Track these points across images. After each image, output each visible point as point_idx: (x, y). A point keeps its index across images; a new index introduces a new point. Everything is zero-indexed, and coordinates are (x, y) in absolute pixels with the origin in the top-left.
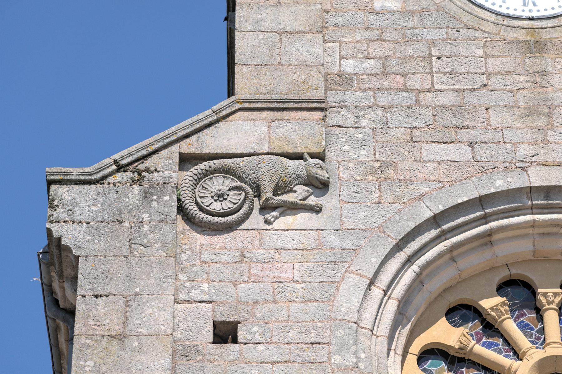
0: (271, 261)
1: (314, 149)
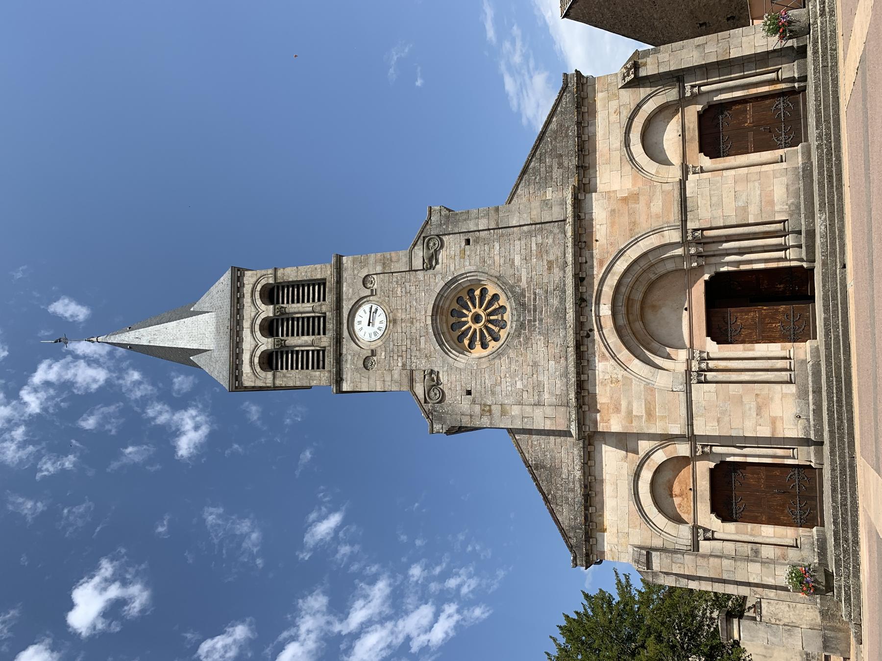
0: (451, 383)
1: (423, 373)
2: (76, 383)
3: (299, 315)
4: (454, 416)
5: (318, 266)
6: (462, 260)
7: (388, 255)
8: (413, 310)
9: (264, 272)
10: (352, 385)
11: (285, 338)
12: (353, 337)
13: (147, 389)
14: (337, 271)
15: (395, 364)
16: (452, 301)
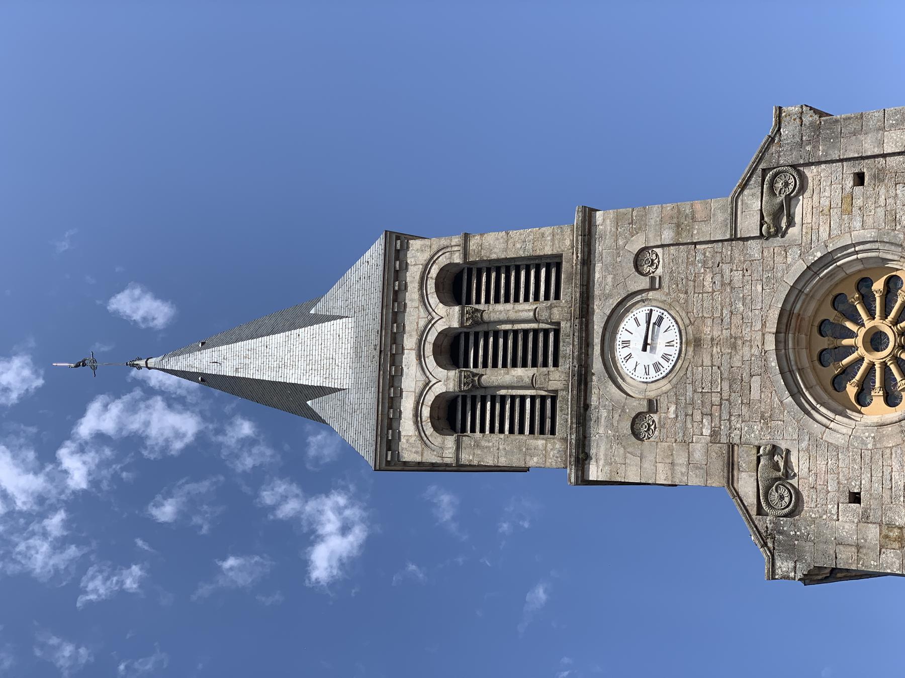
1: (755, 451)
2: (147, 437)
3: (508, 327)
4: (822, 546)
5: (547, 230)
6: (845, 217)
7: (686, 208)
8: (737, 320)
9: (444, 242)
10: (607, 468)
11: (480, 370)
12: (612, 372)
13: (263, 454)
14: (583, 241)
15: (697, 431)
16: (821, 303)
